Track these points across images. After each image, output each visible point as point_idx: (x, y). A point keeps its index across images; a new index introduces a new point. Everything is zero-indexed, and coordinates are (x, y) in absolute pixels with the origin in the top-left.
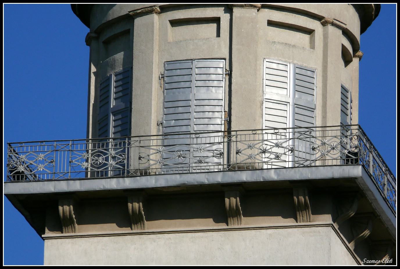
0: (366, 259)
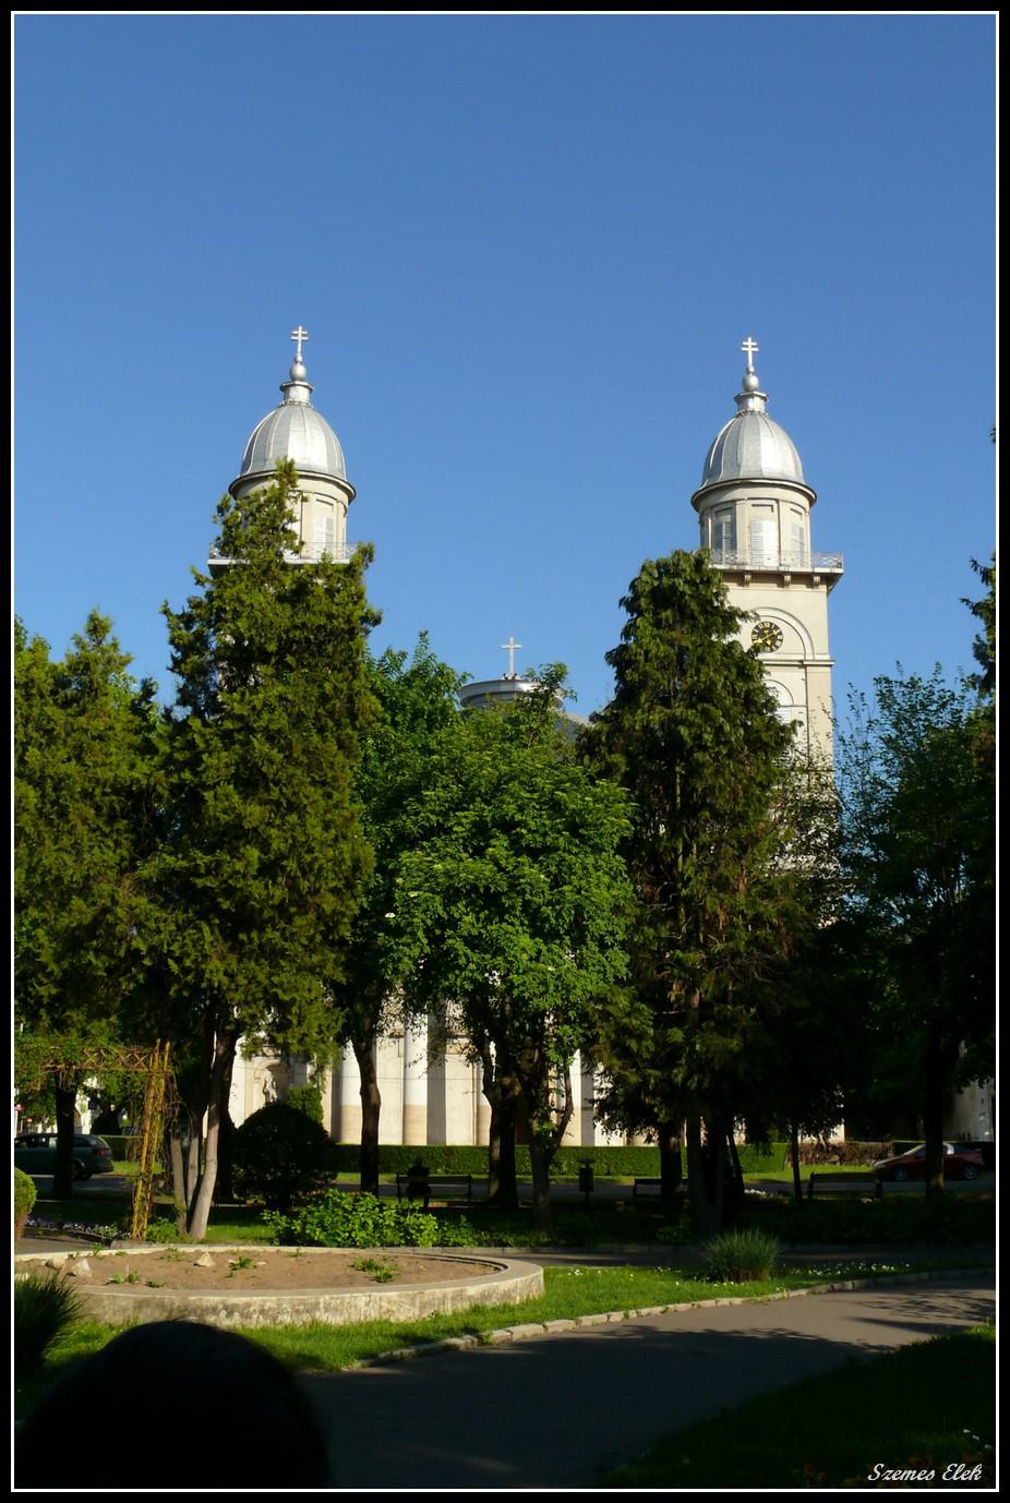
0: (882, 1465)
